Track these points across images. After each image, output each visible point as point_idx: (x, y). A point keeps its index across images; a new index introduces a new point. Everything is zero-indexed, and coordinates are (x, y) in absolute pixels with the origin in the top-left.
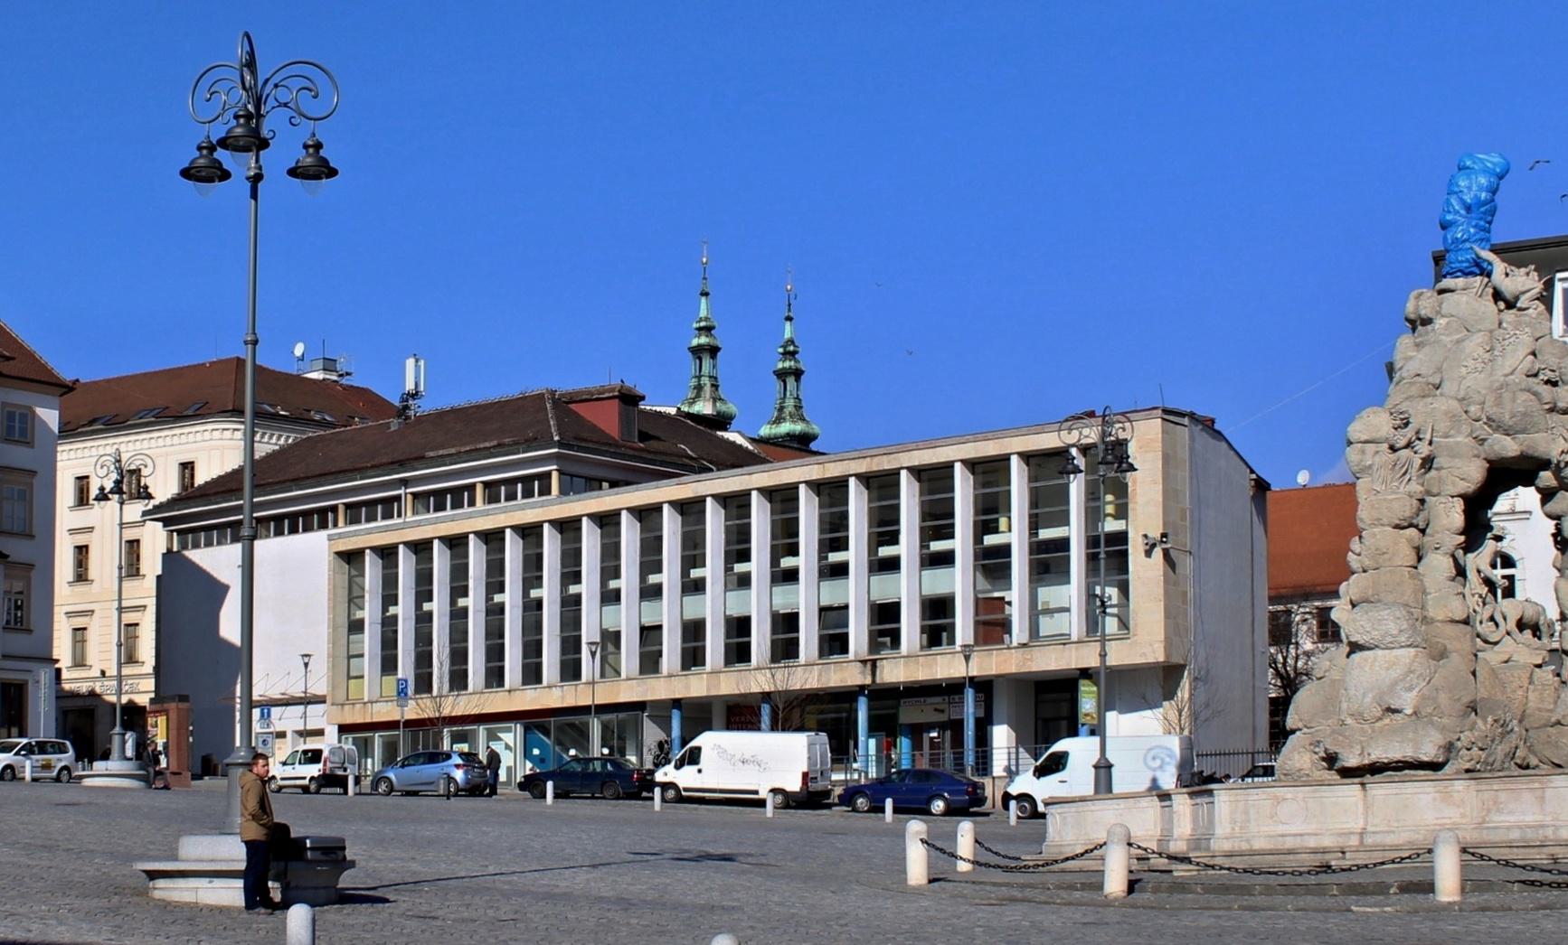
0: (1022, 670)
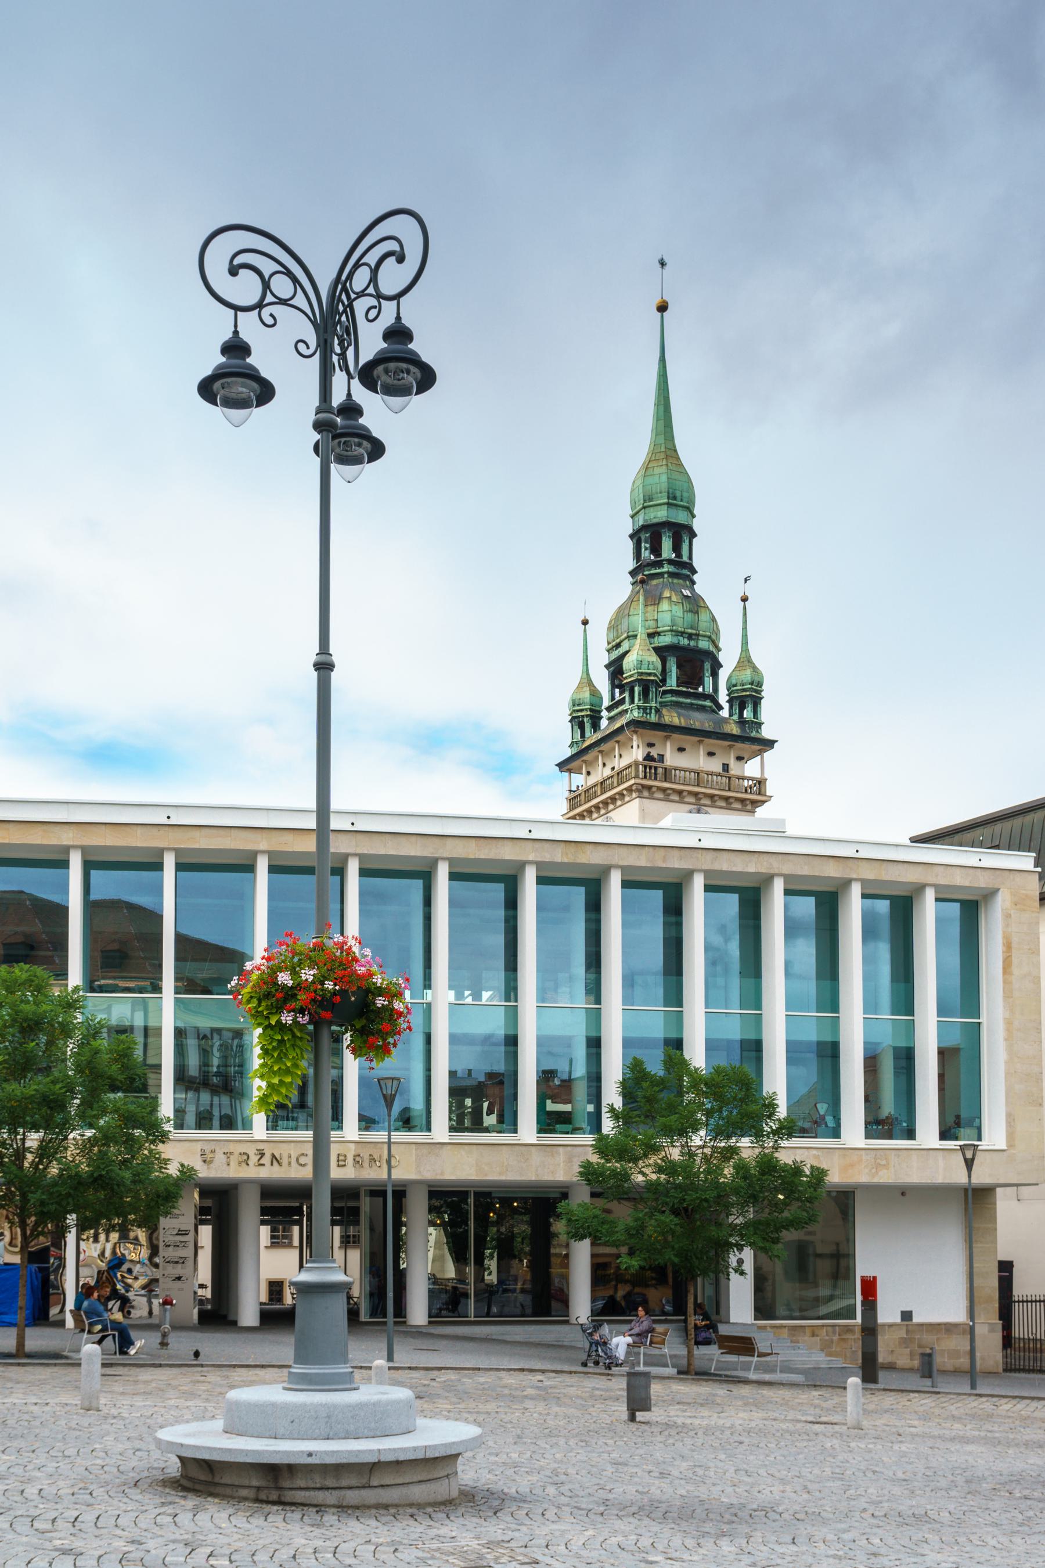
0: (503, 1178)
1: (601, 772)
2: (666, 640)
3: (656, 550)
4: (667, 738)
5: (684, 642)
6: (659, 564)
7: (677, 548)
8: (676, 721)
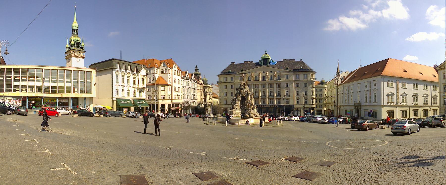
1: (69, 54)
2: (75, 41)
3: (74, 31)
4: (75, 51)
5: (77, 41)
6: (75, 33)
7: (76, 31)
8: (76, 49)
